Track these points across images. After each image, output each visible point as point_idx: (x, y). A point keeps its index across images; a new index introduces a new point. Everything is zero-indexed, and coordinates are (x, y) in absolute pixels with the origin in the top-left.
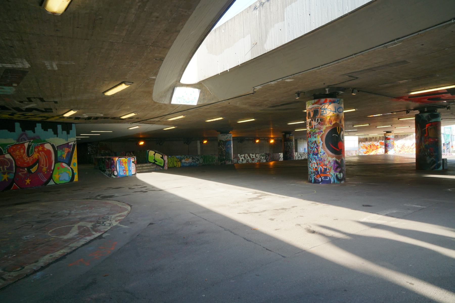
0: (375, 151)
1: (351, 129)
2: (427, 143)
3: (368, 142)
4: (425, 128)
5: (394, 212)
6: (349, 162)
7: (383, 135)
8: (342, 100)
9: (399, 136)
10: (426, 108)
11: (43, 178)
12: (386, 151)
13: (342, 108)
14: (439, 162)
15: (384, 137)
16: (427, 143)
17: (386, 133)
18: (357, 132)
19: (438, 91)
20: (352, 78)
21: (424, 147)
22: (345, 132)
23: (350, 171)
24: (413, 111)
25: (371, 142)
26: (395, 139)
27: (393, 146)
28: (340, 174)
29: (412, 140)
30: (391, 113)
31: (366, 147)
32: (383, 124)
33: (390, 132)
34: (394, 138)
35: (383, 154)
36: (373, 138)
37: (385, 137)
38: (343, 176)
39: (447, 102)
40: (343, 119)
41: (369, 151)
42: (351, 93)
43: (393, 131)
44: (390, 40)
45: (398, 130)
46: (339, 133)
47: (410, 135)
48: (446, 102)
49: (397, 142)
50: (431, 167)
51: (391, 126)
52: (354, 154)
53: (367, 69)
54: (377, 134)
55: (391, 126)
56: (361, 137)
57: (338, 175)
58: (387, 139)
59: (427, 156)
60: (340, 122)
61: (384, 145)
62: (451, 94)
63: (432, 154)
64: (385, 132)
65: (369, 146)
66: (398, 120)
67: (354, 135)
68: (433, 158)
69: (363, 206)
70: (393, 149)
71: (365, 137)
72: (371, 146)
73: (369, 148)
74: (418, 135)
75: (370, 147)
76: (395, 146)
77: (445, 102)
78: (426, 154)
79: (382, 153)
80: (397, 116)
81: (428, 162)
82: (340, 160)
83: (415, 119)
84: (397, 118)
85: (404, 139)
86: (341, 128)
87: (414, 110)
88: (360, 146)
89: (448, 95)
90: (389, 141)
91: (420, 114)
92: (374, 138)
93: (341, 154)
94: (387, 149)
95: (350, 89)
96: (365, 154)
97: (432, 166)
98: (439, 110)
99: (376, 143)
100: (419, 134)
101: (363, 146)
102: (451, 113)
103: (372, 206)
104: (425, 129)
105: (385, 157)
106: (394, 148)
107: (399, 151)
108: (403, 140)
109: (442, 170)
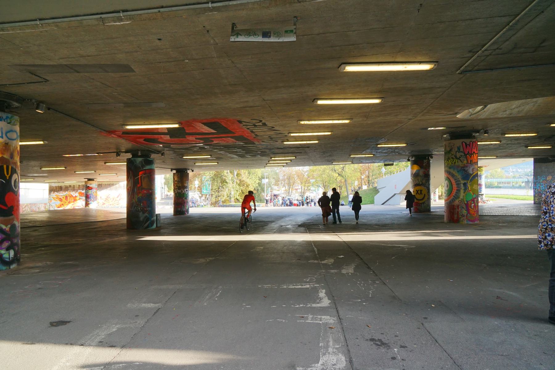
0: (72, 203)
1: (37, 173)
2: (140, 195)
3: (63, 192)
4: (138, 177)
5: (114, 330)
6: (34, 221)
7: (84, 183)
8: (17, 118)
9: (103, 186)
10: (139, 152)
11: (526, 142)
12: (87, 204)
13: (16, 132)
14: (152, 219)
15: (85, 185)
16: (140, 195)
17: (88, 180)
18: (47, 178)
19: (158, 129)
20: (36, 79)
21: (136, 200)
22: (22, 177)
23: (32, 239)
24: (124, 154)
25: (67, 192)
26: (98, 189)
27: (96, 198)
28: (8, 252)
29: (117, 190)
30: (97, 154)
31: (60, 198)
32: (85, 168)
33: (92, 180)
34: (98, 187)
35: (82, 208)
36: (70, 186)
37: (86, 185)
38: (15, 255)
39: (163, 147)
40: (17, 153)
41: (64, 203)
42: (35, 106)
43: (96, 178)
44: (112, 10)
45: (102, 177)
46: (8, 177)
47: (116, 184)
48: (161, 147)
49: (100, 192)
50: (144, 226)
51: (95, 171)
52: (42, 209)
53: (66, 65)
54: (285, 144)
55: (94, 172)
56: (54, 185)
57: (5, 253)
58: (88, 188)
59: (140, 212)
60: (12, 156)
61: (85, 195)
62: (170, 137)
63: (145, 209)
64: (86, 180)
65: (65, 198)
66: (104, 164)
67: (44, 182)
68: (146, 214)
69: (53, 324)
70: (96, 201)
71: (59, 186)
72: (66, 197)
73: (64, 200)
74: (130, 185)
75: (66, 198)
76: (98, 197)
77: (161, 146)
78: (139, 210)
79: (82, 207)
80: (103, 159)
81: (141, 219)
82: (9, 226)
83: (127, 165)
84: (104, 162)
85: (109, 189)
86: (12, 168)
87: (126, 153)
88: (51, 196)
89: (166, 137)
90: (91, 190)
91: (133, 159)
92: (72, 187)
93: (12, 215)
94: (88, 202)
95: (34, 101)
96: (58, 207)
97: (145, 223)
98: (153, 156)
99: (74, 194)
100: (131, 184)
101: (56, 197)
102: (163, 161)
103: (69, 322)
104: (139, 177)
105: (86, 212)
106: (97, 200)
107: (103, 203)
108: (107, 190)
109: (155, 228)
